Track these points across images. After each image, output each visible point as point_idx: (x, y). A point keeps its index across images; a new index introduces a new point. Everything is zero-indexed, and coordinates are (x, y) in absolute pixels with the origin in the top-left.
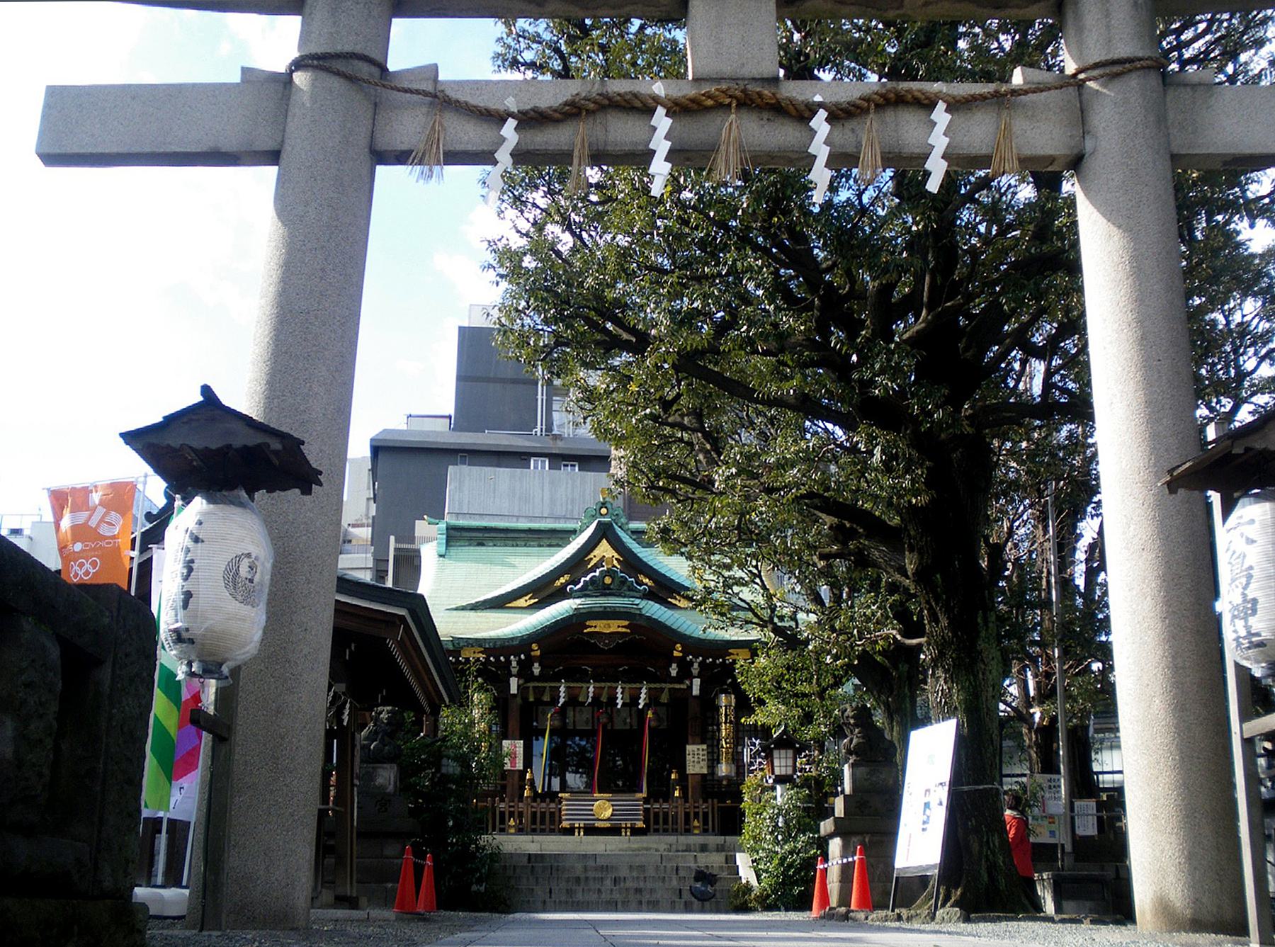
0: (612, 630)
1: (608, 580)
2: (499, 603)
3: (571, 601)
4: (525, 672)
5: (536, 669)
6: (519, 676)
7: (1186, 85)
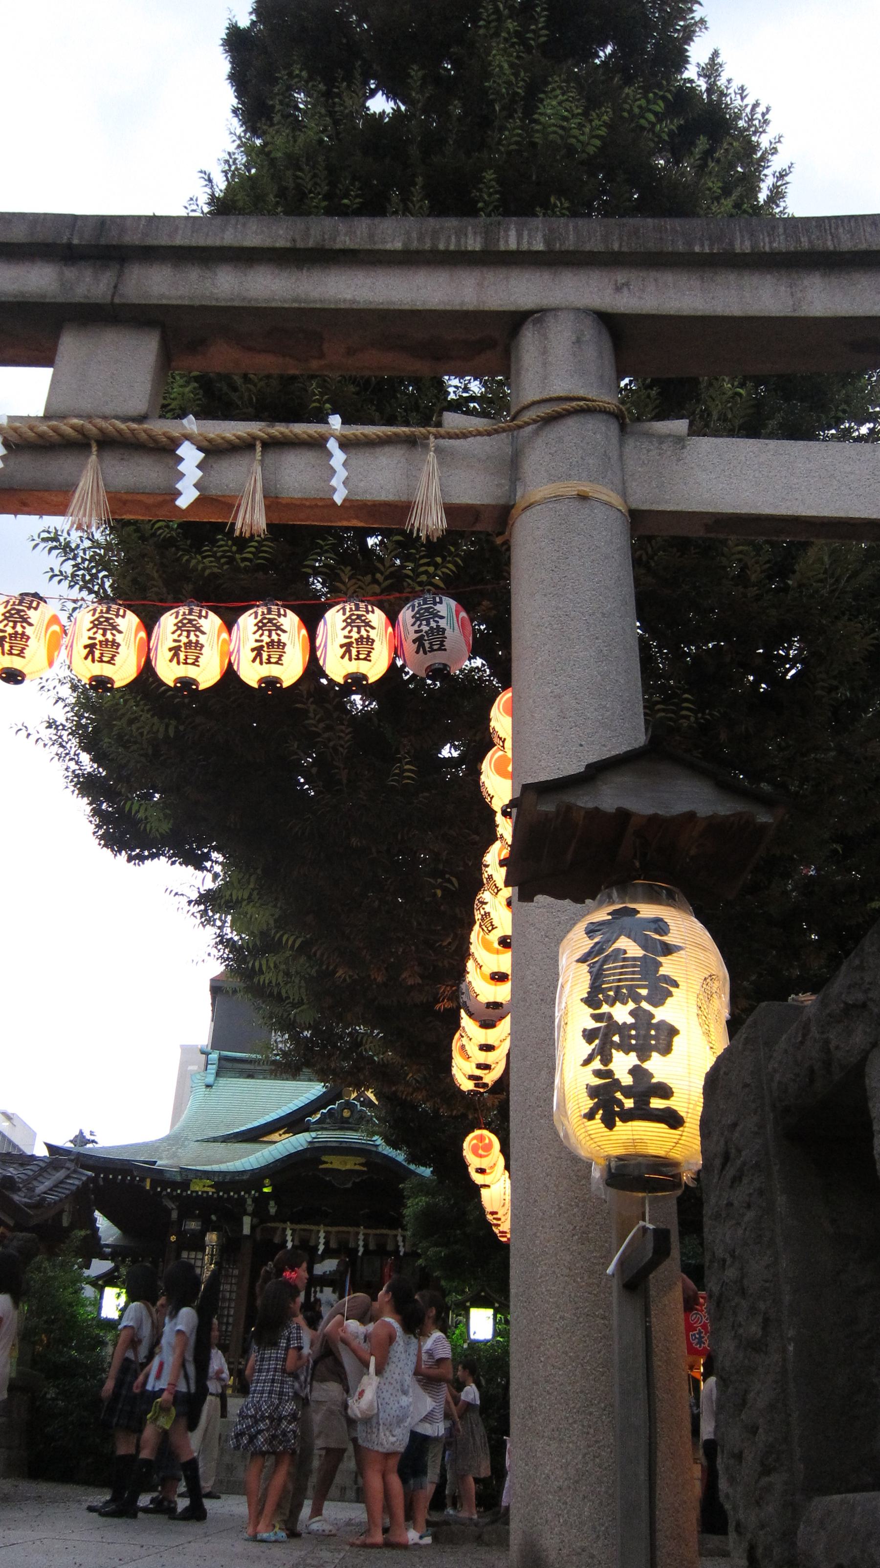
0: (348, 1167)
1: (346, 1113)
2: (255, 1136)
3: (306, 1134)
4: (260, 1213)
5: (273, 1209)
6: (253, 1215)
7: (653, 435)
